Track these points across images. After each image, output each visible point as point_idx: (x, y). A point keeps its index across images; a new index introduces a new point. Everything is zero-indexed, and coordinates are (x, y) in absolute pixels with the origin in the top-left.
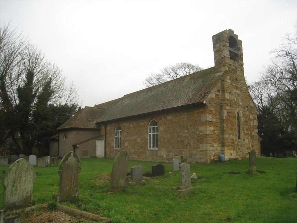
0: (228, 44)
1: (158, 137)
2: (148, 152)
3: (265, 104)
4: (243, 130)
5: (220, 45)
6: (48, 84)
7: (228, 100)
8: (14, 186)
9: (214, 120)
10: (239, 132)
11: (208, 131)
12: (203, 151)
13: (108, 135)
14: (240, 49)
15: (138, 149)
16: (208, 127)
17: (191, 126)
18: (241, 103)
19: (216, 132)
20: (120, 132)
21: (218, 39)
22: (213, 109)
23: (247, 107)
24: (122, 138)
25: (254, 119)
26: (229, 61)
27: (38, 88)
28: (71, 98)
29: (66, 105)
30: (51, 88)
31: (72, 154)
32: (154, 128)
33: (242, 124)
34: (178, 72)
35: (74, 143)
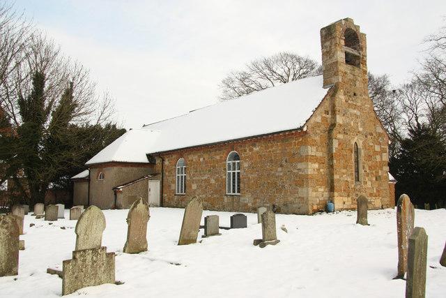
0: (343, 42)
1: (241, 176)
2: (226, 198)
3: (424, 120)
4: (364, 168)
5: (331, 43)
6: (69, 93)
7: (341, 125)
8: (85, 234)
9: (320, 154)
10: (357, 171)
11: (310, 170)
12: (303, 198)
13: (167, 174)
14: (362, 48)
15: (212, 194)
16: (310, 163)
17: (286, 162)
18: (361, 129)
19: (321, 170)
20: (185, 168)
21: (328, 34)
22: (317, 138)
23: (371, 134)
24: (188, 178)
25: (383, 151)
26: (344, 67)
27: (53, 100)
28: (105, 115)
29: (98, 126)
30: (74, 100)
31: (141, 201)
32: (234, 164)
33: (362, 159)
34: (274, 69)
35: (114, 186)
